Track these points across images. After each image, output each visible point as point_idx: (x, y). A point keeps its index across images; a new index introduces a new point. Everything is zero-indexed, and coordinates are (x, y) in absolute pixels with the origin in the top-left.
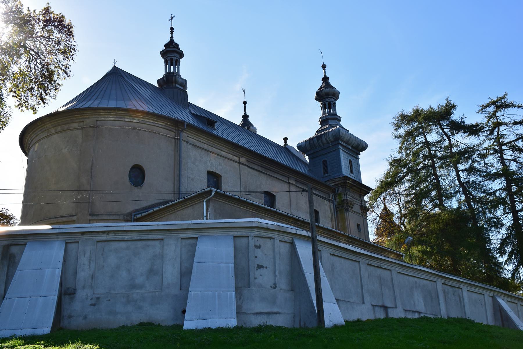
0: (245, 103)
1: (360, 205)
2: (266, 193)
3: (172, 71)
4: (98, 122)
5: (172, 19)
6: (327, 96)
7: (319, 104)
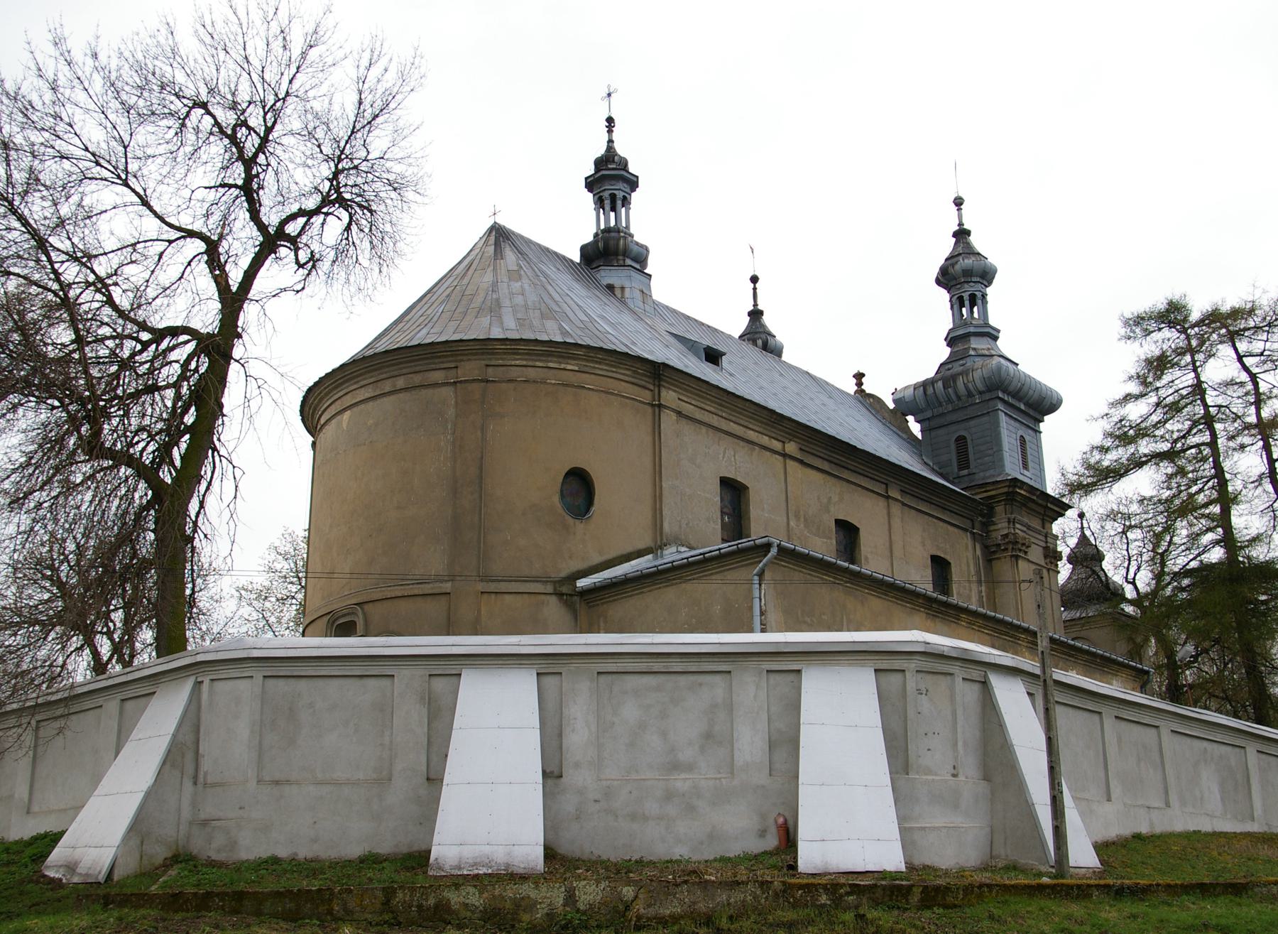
0: (754, 279)
1: (1043, 544)
2: (841, 524)
3: (612, 223)
4: (490, 370)
5: (609, 95)
6: (965, 277)
7: (943, 296)
